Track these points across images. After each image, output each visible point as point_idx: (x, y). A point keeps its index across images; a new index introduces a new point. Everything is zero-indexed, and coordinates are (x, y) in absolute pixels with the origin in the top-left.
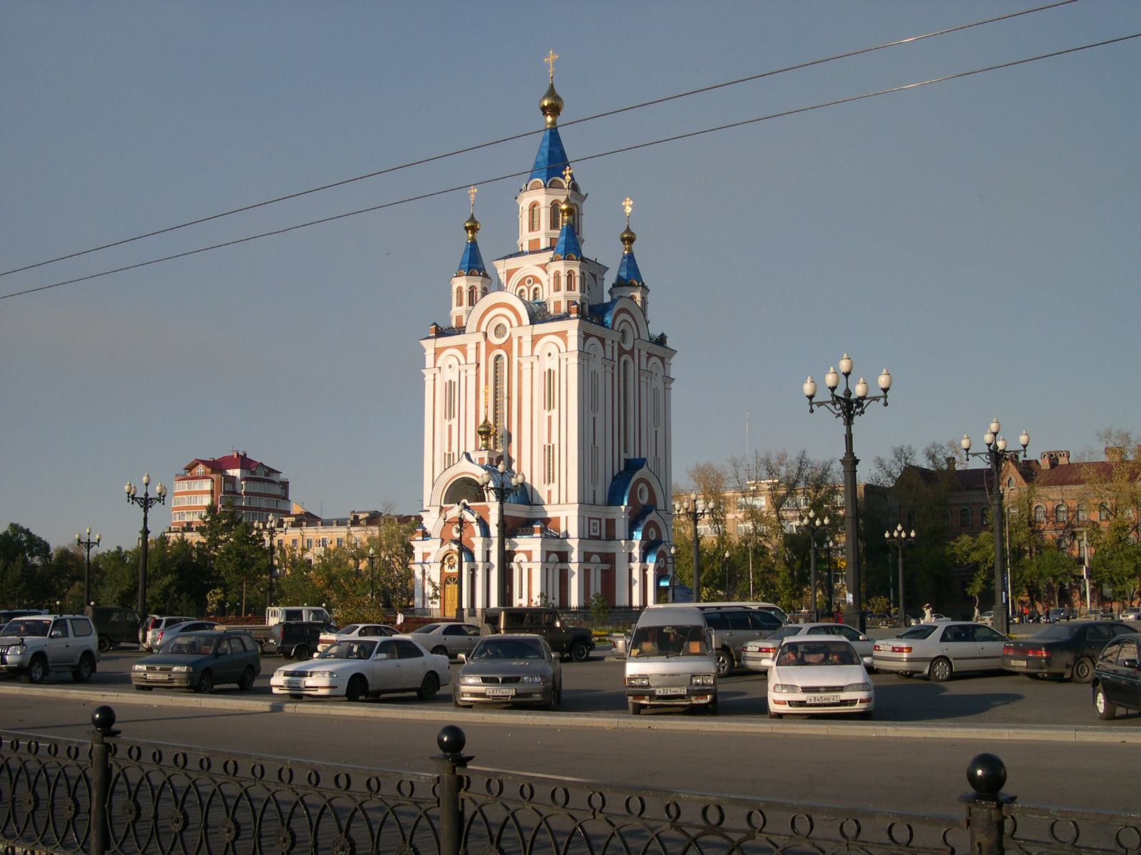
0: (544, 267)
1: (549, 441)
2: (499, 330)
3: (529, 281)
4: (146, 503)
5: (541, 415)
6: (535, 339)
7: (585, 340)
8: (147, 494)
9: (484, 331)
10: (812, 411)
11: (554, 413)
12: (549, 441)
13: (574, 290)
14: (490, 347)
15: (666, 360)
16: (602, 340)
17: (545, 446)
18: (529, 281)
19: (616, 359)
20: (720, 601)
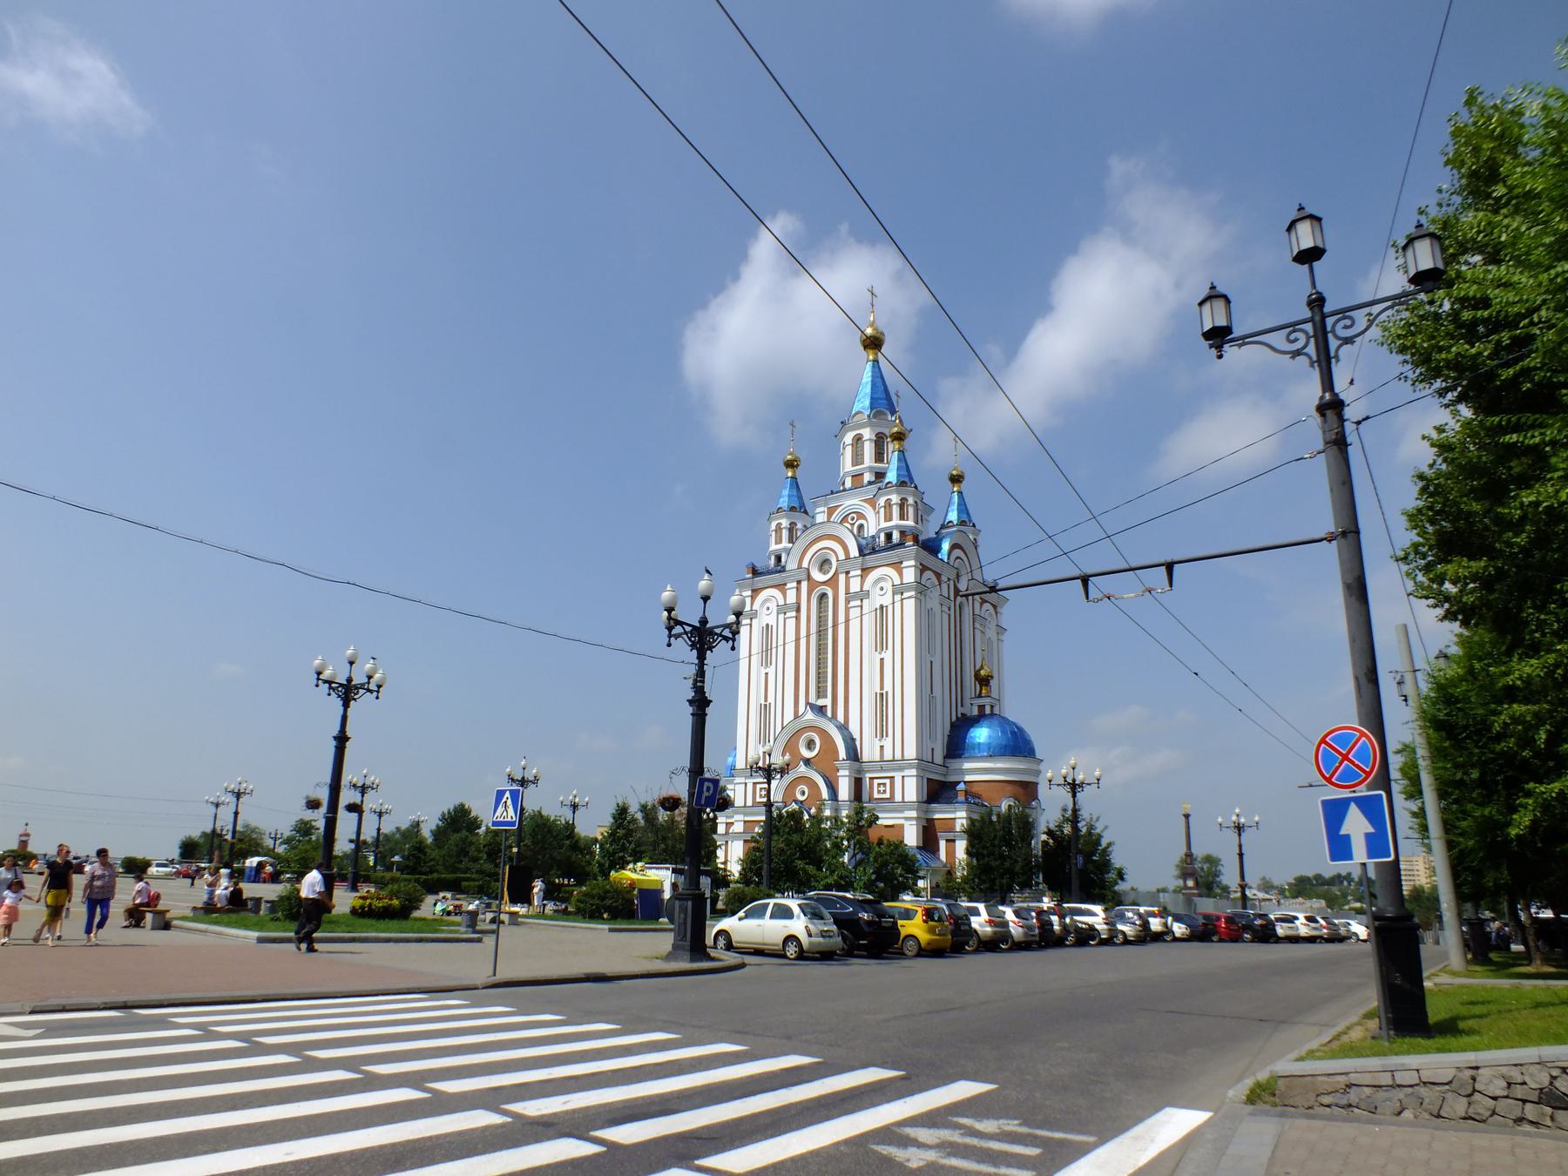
3: (853, 519)
4: (348, 692)
5: (872, 658)
7: (922, 572)
8: (350, 680)
9: (807, 567)
10: (317, 686)
11: (887, 655)
13: (907, 520)
15: (998, 609)
16: (938, 575)
17: (876, 693)
18: (853, 519)
19: (952, 598)
20: (1444, 811)
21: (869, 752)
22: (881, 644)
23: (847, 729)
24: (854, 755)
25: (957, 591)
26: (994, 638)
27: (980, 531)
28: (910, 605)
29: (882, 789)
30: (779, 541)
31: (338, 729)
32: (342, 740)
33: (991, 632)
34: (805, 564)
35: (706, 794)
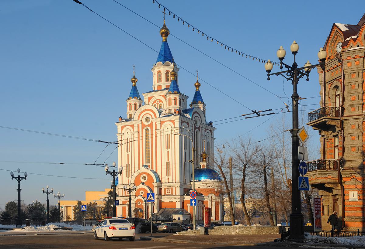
0: (164, 96)
1: (168, 160)
2: (147, 119)
6: (162, 123)
8: (19, 176)
12: (168, 160)
14: (143, 126)
15: (212, 132)
16: (188, 124)
19: (193, 130)
21: (164, 179)
22: (168, 147)
23: (157, 173)
24: (159, 180)
25: (195, 128)
26: (210, 142)
27: (206, 105)
28: (177, 137)
29: (169, 191)
30: (130, 109)
31: (18, 187)
32: (19, 190)
33: (209, 140)
34: (140, 119)
35: (116, 203)
